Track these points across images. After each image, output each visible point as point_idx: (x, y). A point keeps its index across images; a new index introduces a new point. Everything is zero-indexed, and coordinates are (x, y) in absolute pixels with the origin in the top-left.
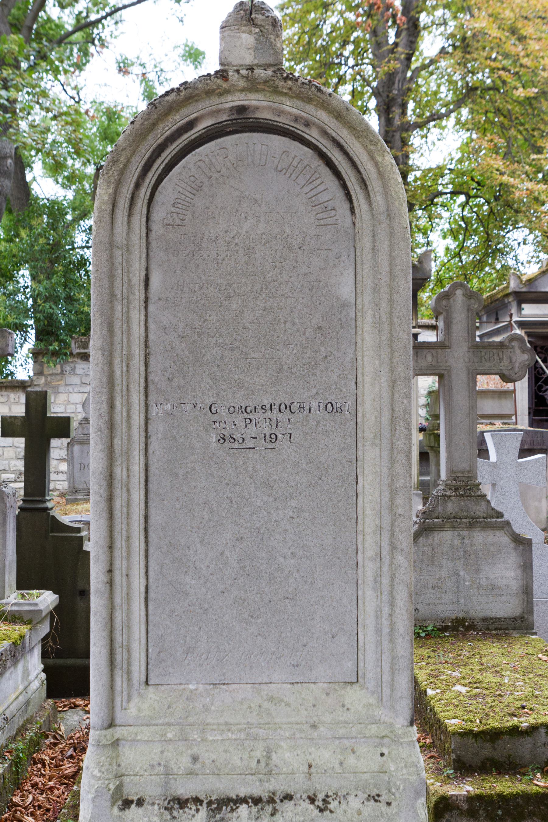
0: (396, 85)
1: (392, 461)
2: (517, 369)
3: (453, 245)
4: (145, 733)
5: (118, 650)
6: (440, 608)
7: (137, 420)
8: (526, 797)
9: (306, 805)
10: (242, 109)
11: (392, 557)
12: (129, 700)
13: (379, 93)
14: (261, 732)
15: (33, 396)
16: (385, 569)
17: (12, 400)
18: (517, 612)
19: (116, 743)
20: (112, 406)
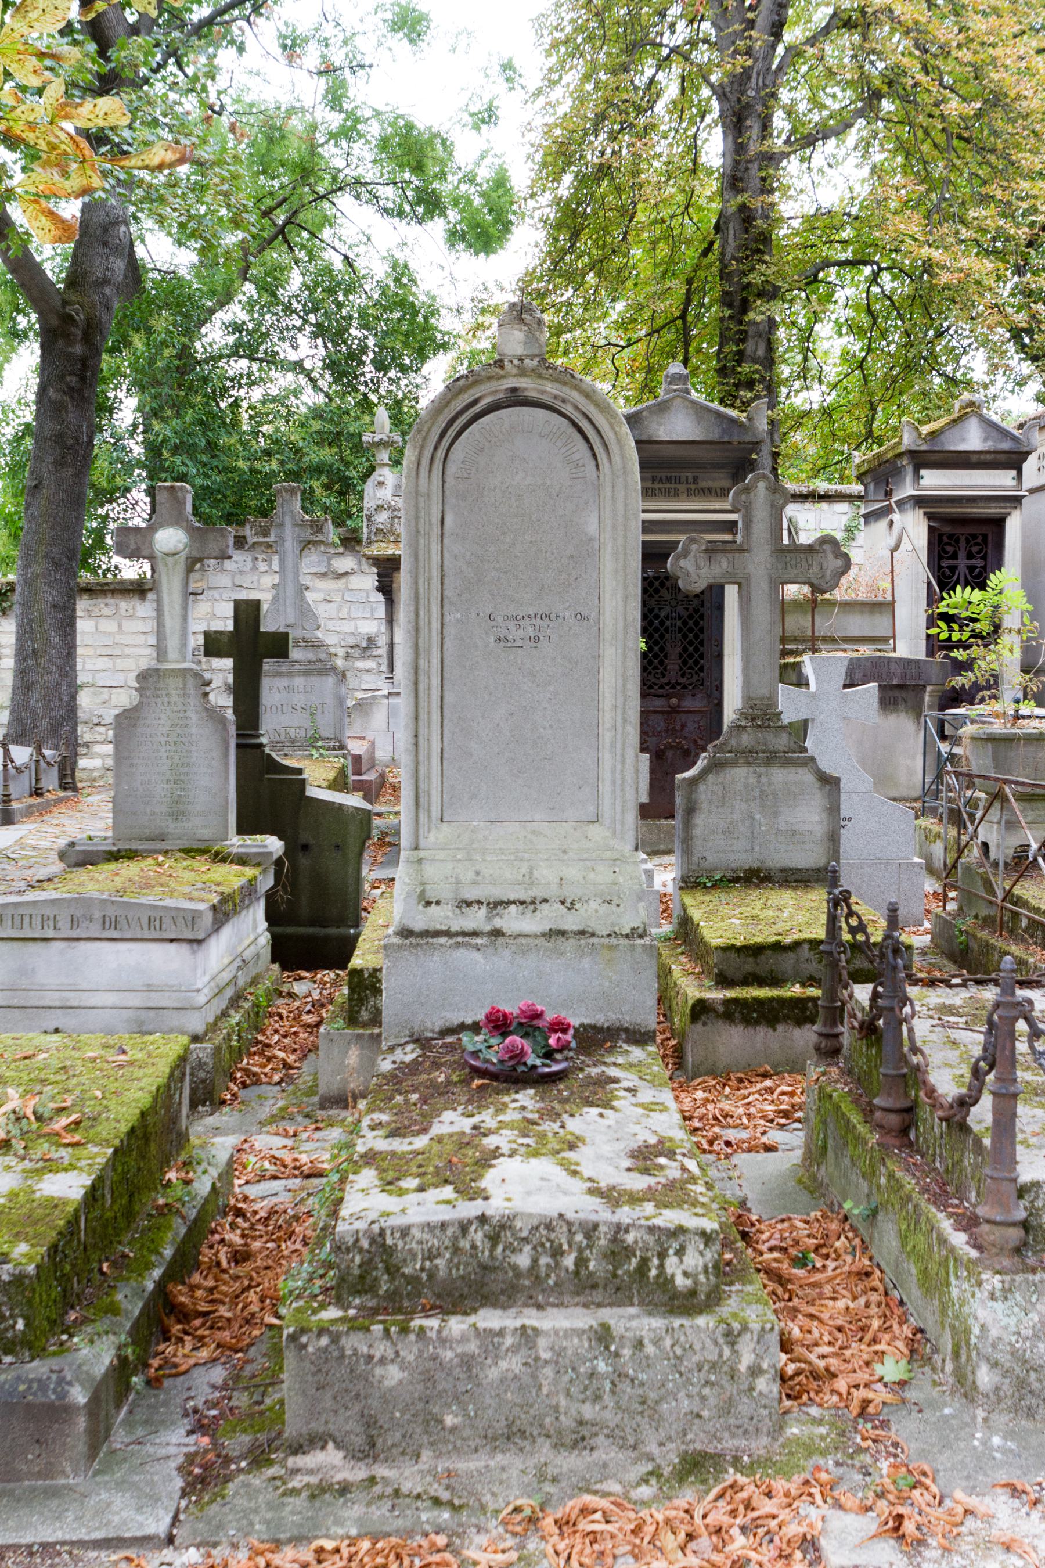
0: (754, 80)
1: (625, 656)
2: (828, 578)
3: (857, 347)
4: (441, 855)
5: (422, 795)
6: (732, 857)
7: (436, 625)
8: (782, 1001)
9: (559, 905)
10: (514, 390)
11: (624, 727)
12: (429, 831)
13: (724, 94)
14: (527, 856)
15: (243, 607)
16: (619, 737)
17: (123, 612)
18: (821, 862)
19: (420, 861)
20: (417, 615)
